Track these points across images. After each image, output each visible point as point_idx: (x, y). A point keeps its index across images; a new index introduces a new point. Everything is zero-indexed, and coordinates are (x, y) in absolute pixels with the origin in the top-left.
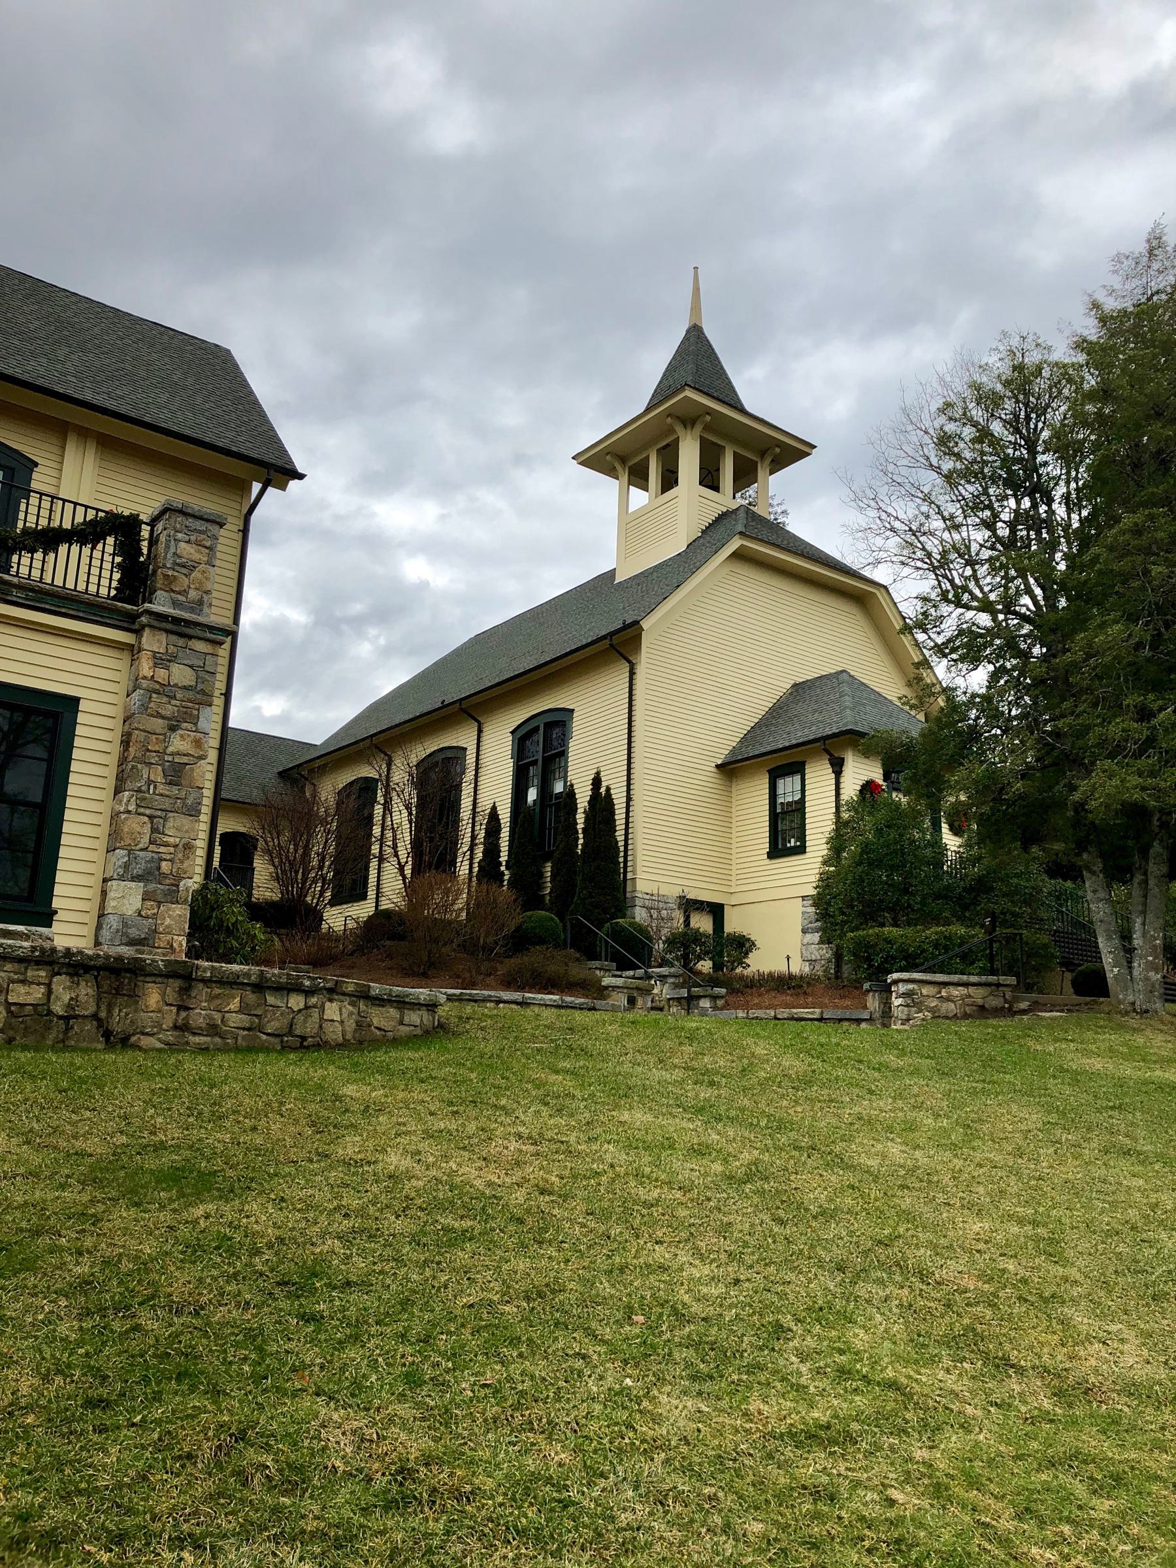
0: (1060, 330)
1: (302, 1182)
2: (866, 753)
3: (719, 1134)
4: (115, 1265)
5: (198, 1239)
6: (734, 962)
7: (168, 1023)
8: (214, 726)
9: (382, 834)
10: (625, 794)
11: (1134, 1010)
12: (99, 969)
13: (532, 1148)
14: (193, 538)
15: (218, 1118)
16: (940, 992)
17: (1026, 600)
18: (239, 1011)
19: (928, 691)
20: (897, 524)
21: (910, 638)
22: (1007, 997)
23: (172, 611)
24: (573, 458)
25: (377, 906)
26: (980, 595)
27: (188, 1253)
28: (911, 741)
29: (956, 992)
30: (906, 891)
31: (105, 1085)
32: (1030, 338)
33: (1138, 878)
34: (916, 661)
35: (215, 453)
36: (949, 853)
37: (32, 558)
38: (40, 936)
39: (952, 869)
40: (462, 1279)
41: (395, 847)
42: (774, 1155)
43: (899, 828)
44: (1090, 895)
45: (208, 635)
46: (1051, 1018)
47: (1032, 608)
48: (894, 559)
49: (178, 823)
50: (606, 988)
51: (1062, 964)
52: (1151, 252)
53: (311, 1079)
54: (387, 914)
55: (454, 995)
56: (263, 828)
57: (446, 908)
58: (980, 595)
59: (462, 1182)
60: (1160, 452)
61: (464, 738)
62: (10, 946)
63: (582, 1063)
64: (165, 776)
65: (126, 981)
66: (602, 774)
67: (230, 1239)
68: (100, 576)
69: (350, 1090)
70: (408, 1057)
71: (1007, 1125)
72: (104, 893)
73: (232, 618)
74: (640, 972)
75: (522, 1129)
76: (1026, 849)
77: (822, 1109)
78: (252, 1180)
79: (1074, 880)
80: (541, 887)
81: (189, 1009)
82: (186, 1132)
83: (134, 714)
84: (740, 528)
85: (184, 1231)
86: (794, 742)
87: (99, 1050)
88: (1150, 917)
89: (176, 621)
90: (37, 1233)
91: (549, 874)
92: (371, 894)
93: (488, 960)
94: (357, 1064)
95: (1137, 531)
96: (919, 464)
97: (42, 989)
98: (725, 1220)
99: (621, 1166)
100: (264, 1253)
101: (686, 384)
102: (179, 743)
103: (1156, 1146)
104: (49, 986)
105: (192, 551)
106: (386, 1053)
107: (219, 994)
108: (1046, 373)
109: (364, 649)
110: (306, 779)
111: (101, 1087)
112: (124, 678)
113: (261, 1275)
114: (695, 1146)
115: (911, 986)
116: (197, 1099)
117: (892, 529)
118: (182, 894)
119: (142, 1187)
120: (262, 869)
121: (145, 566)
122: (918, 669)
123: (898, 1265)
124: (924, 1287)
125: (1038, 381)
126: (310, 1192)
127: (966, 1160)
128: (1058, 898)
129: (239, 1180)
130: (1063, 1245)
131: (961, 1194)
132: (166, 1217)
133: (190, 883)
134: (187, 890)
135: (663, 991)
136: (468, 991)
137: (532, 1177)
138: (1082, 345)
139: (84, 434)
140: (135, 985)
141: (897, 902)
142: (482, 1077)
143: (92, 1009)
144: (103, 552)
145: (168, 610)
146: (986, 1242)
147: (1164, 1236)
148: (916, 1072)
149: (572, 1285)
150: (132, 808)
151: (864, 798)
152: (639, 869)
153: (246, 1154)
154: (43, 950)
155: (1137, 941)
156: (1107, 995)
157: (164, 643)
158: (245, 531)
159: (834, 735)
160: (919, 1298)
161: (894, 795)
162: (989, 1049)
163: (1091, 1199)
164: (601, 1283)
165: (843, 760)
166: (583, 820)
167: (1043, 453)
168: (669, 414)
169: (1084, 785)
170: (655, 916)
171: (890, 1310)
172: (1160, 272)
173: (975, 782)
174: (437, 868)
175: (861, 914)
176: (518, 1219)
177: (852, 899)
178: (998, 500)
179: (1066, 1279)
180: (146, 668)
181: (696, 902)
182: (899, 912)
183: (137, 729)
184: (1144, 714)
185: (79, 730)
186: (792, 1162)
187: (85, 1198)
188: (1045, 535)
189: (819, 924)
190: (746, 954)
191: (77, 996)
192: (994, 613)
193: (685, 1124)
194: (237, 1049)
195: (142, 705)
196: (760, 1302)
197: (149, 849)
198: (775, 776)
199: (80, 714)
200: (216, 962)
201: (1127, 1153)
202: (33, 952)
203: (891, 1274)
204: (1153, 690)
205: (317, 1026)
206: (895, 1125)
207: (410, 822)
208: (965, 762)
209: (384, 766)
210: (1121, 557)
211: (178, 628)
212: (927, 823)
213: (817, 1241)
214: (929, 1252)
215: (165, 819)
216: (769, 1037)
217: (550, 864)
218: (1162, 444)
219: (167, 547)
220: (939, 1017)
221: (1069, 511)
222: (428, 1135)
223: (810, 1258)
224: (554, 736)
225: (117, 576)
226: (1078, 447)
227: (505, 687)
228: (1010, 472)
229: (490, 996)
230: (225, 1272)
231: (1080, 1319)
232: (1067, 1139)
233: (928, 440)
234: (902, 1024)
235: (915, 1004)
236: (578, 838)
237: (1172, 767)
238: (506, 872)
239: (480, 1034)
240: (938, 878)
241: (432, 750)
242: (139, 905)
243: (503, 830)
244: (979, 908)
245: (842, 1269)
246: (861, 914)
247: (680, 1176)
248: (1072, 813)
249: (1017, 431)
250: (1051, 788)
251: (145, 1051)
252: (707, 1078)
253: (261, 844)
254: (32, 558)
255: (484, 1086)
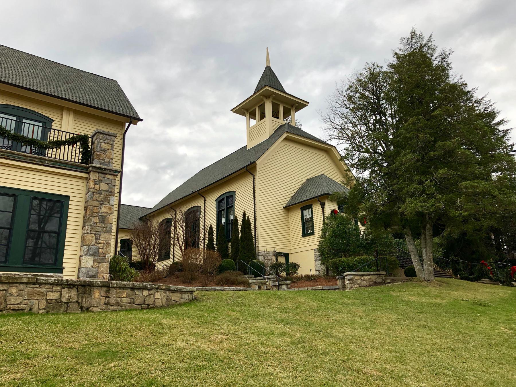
0: (385, 62)
1: (148, 353)
2: (332, 200)
3: (289, 329)
4: (82, 385)
5: (112, 374)
6: (293, 272)
7: (102, 302)
8: (115, 203)
9: (174, 236)
10: (254, 218)
11: (425, 280)
12: (78, 285)
13: (226, 337)
14: (106, 142)
15: (119, 333)
16: (361, 278)
17: (380, 148)
18: (127, 297)
19: (350, 179)
20: (337, 127)
21: (343, 162)
22: (383, 278)
23: (100, 166)
24: (231, 110)
25: (173, 261)
26: (365, 147)
27: (108, 379)
28: (346, 195)
29: (366, 278)
30: (348, 245)
31: (80, 325)
32: (376, 64)
33: (423, 236)
34: (346, 169)
35: (113, 114)
36: (361, 232)
37: (52, 151)
38: (59, 276)
39: (363, 237)
40: (203, 382)
41: (178, 240)
42: (307, 334)
43: (344, 225)
44: (408, 243)
45: (112, 173)
46: (398, 284)
47: (382, 150)
48: (337, 138)
49: (104, 236)
50: (251, 283)
51: (400, 267)
52: (412, 36)
53: (151, 318)
54: (177, 263)
55: (200, 289)
56: (134, 237)
57: (196, 259)
58: (365, 147)
59: (202, 349)
60: (419, 98)
61: (200, 203)
62: (47, 280)
63: (242, 308)
64: (99, 220)
65: (87, 289)
66: (246, 212)
67: (123, 374)
68: (75, 156)
69: (164, 321)
70: (183, 309)
71: (385, 320)
72: (80, 261)
73: (120, 168)
74: (262, 278)
75: (222, 331)
76: (386, 229)
77: (323, 319)
78: (131, 353)
79: (403, 239)
80: (228, 251)
81: (109, 297)
82: (108, 338)
83: (88, 200)
84: (286, 130)
85: (107, 372)
86: (308, 198)
87: (79, 313)
88: (428, 249)
89: (101, 169)
90: (56, 376)
91: (230, 246)
92: (172, 257)
93: (211, 276)
94: (166, 313)
95: (414, 124)
96: (343, 107)
97: (59, 294)
98: (292, 357)
99: (256, 341)
100: (134, 378)
101: (266, 85)
102: (103, 209)
103: (434, 324)
104: (61, 292)
105: (106, 146)
106: (176, 308)
107: (119, 292)
108: (381, 75)
109: (166, 177)
110: (148, 220)
111: (79, 325)
112: (84, 189)
113: (133, 385)
114: (281, 333)
115: (351, 277)
116: (112, 327)
117: (336, 128)
118: (107, 259)
119: (92, 358)
120: (134, 250)
121: (90, 151)
122: (346, 172)
123: (350, 368)
124: (359, 375)
125: (379, 78)
126: (151, 356)
127: (372, 332)
128: (398, 245)
129: (126, 353)
130: (405, 358)
131: (370, 344)
132: (100, 368)
133: (109, 255)
134: (108, 258)
135: (269, 283)
136: (205, 287)
137: (226, 346)
138: (392, 66)
139: (69, 110)
140: (91, 290)
141: (345, 250)
142: (209, 314)
143: (76, 299)
144: (76, 148)
145: (99, 165)
146: (379, 359)
147: (439, 354)
148: (354, 304)
149: (240, 382)
150: (89, 231)
151: (332, 215)
152: (260, 243)
153: (129, 344)
154: (58, 280)
155: (424, 257)
156: (416, 276)
157: (98, 176)
158: (124, 139)
159: (321, 195)
160: (357, 379)
161: (342, 214)
162: (378, 296)
163: (414, 343)
164: (250, 380)
165: (324, 203)
166: (240, 228)
167: (382, 101)
168: (261, 95)
169: (403, 207)
170: (266, 258)
171: (348, 384)
172: (415, 43)
173: (367, 208)
174: (193, 246)
175: (333, 254)
176: (222, 361)
177: (330, 249)
178: (368, 116)
179: (406, 370)
180: (92, 185)
181: (279, 253)
182: (346, 252)
183: (89, 205)
184: (421, 183)
185: (70, 207)
186: (314, 336)
187: (73, 363)
188: (385, 127)
189: (320, 258)
190: (297, 269)
191: (71, 295)
192: (371, 153)
193: (277, 326)
194: (126, 310)
195: (91, 197)
196: (304, 383)
197: (95, 245)
198: (303, 209)
199: (70, 201)
200: (118, 281)
201: (425, 327)
202: (55, 281)
203: (347, 371)
204: (423, 175)
205: (153, 301)
206: (348, 322)
207: (183, 232)
208: (364, 201)
209: (173, 214)
210: (409, 133)
211: (102, 171)
212: (353, 222)
213: (323, 362)
214: (360, 364)
215: (100, 235)
216: (305, 296)
217: (230, 243)
218: (420, 96)
219: (97, 145)
220: (361, 286)
221: (392, 119)
222: (191, 334)
223: (320, 368)
224: (230, 201)
225: (81, 156)
226: (394, 99)
227: (212, 186)
228: (372, 107)
229: (212, 288)
230: (121, 385)
231: (412, 383)
232: (405, 324)
233: (345, 99)
234: (349, 289)
235: (353, 283)
236: (239, 234)
237: (431, 199)
238: (216, 247)
239: (208, 301)
240: (358, 240)
241: (189, 208)
242: (92, 264)
243: (214, 233)
244: (372, 250)
245: (331, 371)
246: (333, 254)
247: (276, 343)
248: (400, 216)
249: (373, 94)
250: (392, 208)
251: (95, 313)
252: (285, 310)
253: (134, 242)
254: (52, 151)
255: (210, 317)
